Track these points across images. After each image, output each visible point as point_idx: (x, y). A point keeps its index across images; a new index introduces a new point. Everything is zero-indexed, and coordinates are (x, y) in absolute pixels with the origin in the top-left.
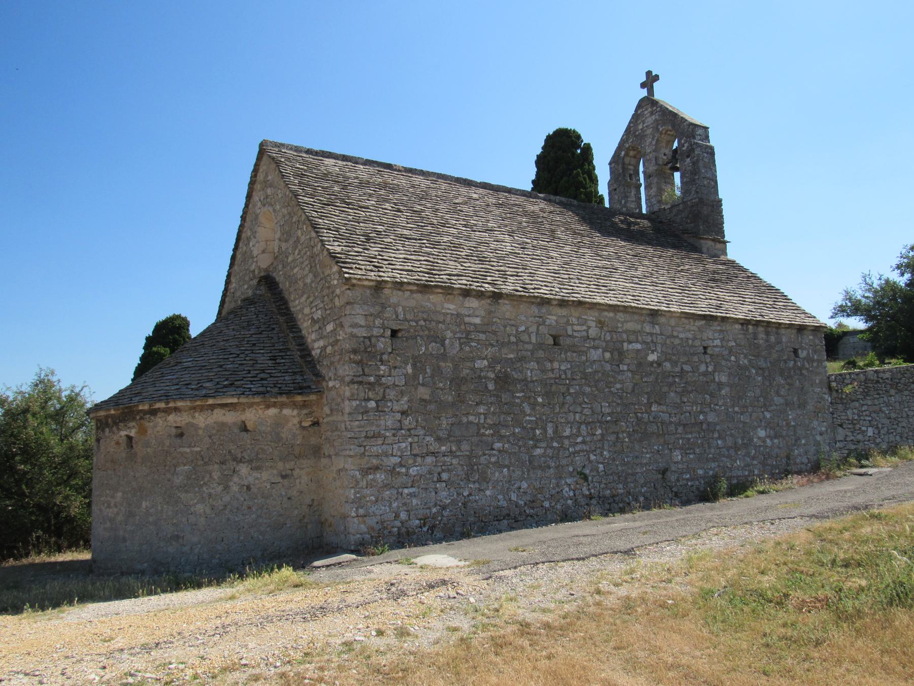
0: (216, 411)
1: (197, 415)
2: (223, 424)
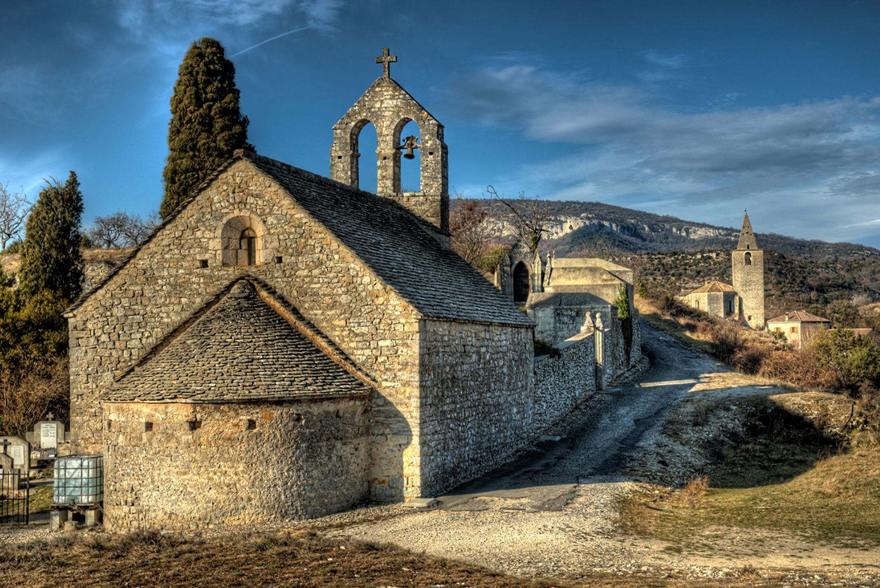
0: (325, 403)
1: (312, 405)
2: (328, 413)
